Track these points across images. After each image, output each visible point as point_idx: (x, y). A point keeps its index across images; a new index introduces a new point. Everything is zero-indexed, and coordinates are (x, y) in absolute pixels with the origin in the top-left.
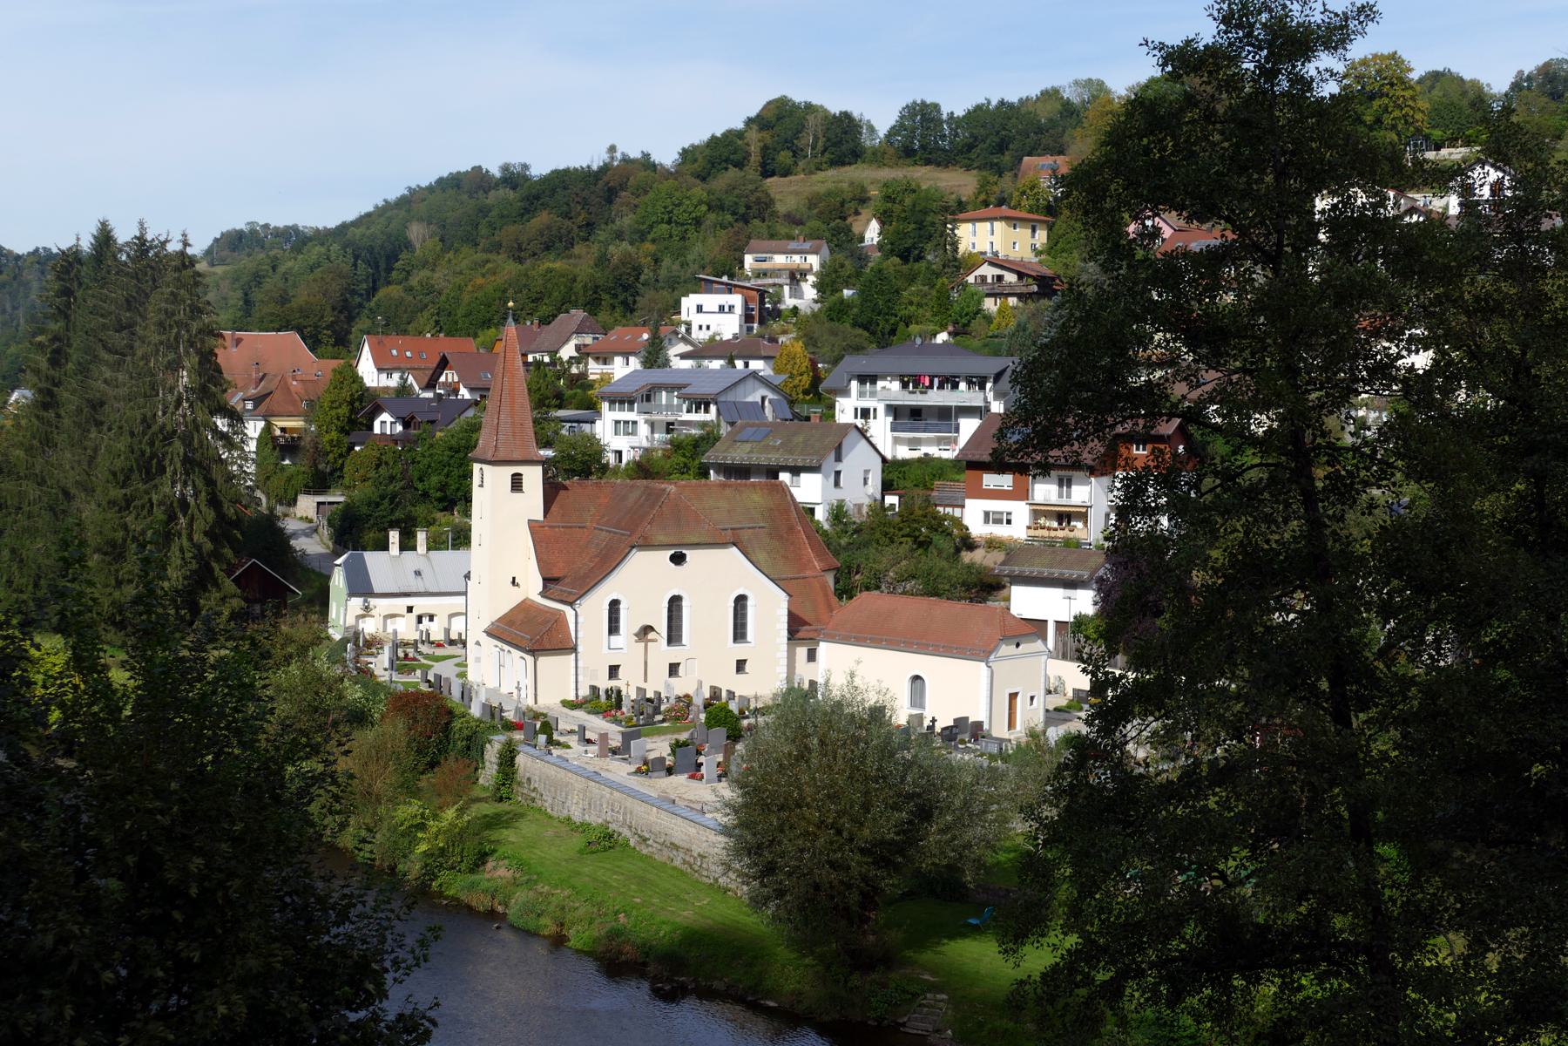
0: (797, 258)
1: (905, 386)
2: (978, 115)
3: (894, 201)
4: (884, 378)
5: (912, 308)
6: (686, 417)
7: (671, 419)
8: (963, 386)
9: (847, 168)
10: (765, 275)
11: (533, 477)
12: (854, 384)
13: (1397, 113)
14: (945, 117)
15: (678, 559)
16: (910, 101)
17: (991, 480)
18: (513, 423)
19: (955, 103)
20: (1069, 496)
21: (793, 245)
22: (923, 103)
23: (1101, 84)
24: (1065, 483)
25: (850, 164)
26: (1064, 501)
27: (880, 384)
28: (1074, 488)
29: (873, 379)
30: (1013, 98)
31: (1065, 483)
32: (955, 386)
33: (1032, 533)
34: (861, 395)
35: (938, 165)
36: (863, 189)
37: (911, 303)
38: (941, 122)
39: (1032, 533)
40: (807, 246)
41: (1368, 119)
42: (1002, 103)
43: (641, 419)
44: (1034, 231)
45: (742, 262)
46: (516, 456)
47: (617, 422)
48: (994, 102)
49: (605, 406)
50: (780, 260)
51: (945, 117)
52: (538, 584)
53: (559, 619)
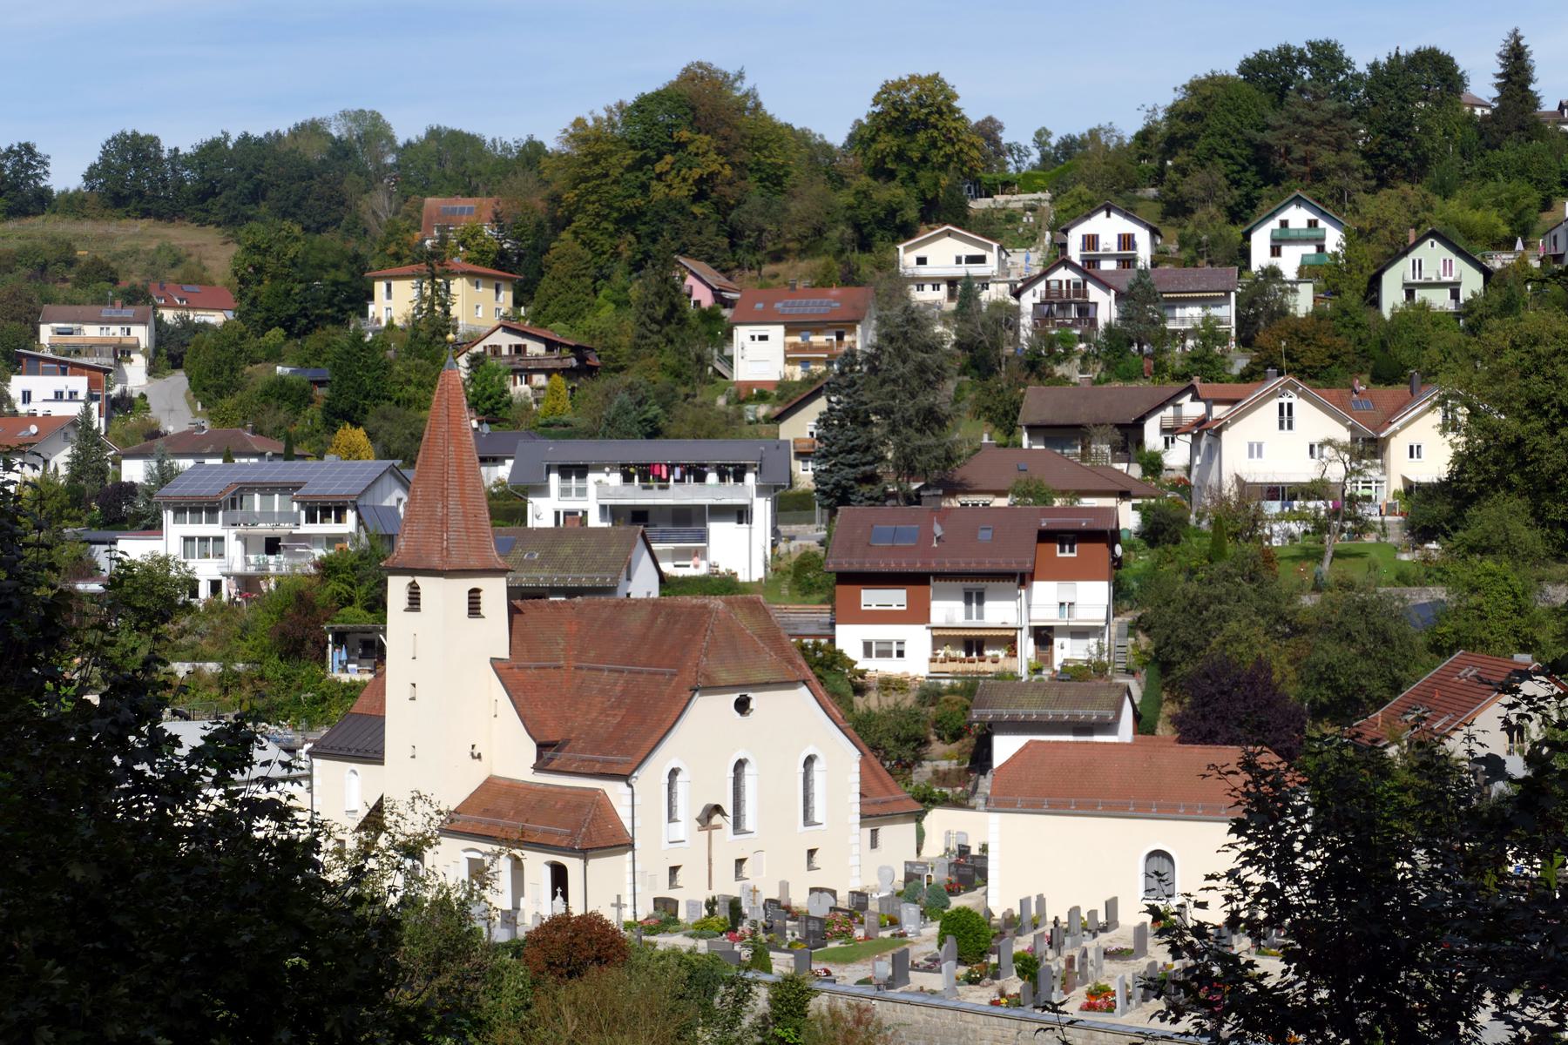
0: (116, 330)
1: (628, 478)
2: (212, 151)
3: (265, 252)
4: (599, 468)
5: (412, 389)
6: (306, 529)
7: (278, 532)
8: (712, 478)
9: (31, 220)
10: (78, 352)
11: (495, 592)
12: (554, 478)
13: (948, 149)
14: (165, 155)
15: (742, 706)
16: (117, 131)
17: (872, 598)
18: (465, 515)
19: (180, 135)
20: (980, 616)
21: (106, 312)
22: (135, 134)
23: (376, 117)
24: (975, 598)
25: (35, 214)
26: (974, 622)
27: (592, 477)
28: (988, 605)
29: (582, 471)
30: (258, 132)
31: (975, 598)
32: (700, 478)
33: (937, 667)
34: (565, 492)
35: (159, 217)
36: (70, 248)
37: (409, 382)
38: (158, 159)
39: (937, 667)
40: (129, 312)
41: (916, 155)
42: (245, 138)
43: (230, 534)
44: (498, 292)
45: (36, 333)
46: (474, 563)
47: (188, 539)
48: (745, 86)
49: (168, 516)
50: (92, 332)
51: (165, 155)
52: (530, 751)
53: (600, 803)
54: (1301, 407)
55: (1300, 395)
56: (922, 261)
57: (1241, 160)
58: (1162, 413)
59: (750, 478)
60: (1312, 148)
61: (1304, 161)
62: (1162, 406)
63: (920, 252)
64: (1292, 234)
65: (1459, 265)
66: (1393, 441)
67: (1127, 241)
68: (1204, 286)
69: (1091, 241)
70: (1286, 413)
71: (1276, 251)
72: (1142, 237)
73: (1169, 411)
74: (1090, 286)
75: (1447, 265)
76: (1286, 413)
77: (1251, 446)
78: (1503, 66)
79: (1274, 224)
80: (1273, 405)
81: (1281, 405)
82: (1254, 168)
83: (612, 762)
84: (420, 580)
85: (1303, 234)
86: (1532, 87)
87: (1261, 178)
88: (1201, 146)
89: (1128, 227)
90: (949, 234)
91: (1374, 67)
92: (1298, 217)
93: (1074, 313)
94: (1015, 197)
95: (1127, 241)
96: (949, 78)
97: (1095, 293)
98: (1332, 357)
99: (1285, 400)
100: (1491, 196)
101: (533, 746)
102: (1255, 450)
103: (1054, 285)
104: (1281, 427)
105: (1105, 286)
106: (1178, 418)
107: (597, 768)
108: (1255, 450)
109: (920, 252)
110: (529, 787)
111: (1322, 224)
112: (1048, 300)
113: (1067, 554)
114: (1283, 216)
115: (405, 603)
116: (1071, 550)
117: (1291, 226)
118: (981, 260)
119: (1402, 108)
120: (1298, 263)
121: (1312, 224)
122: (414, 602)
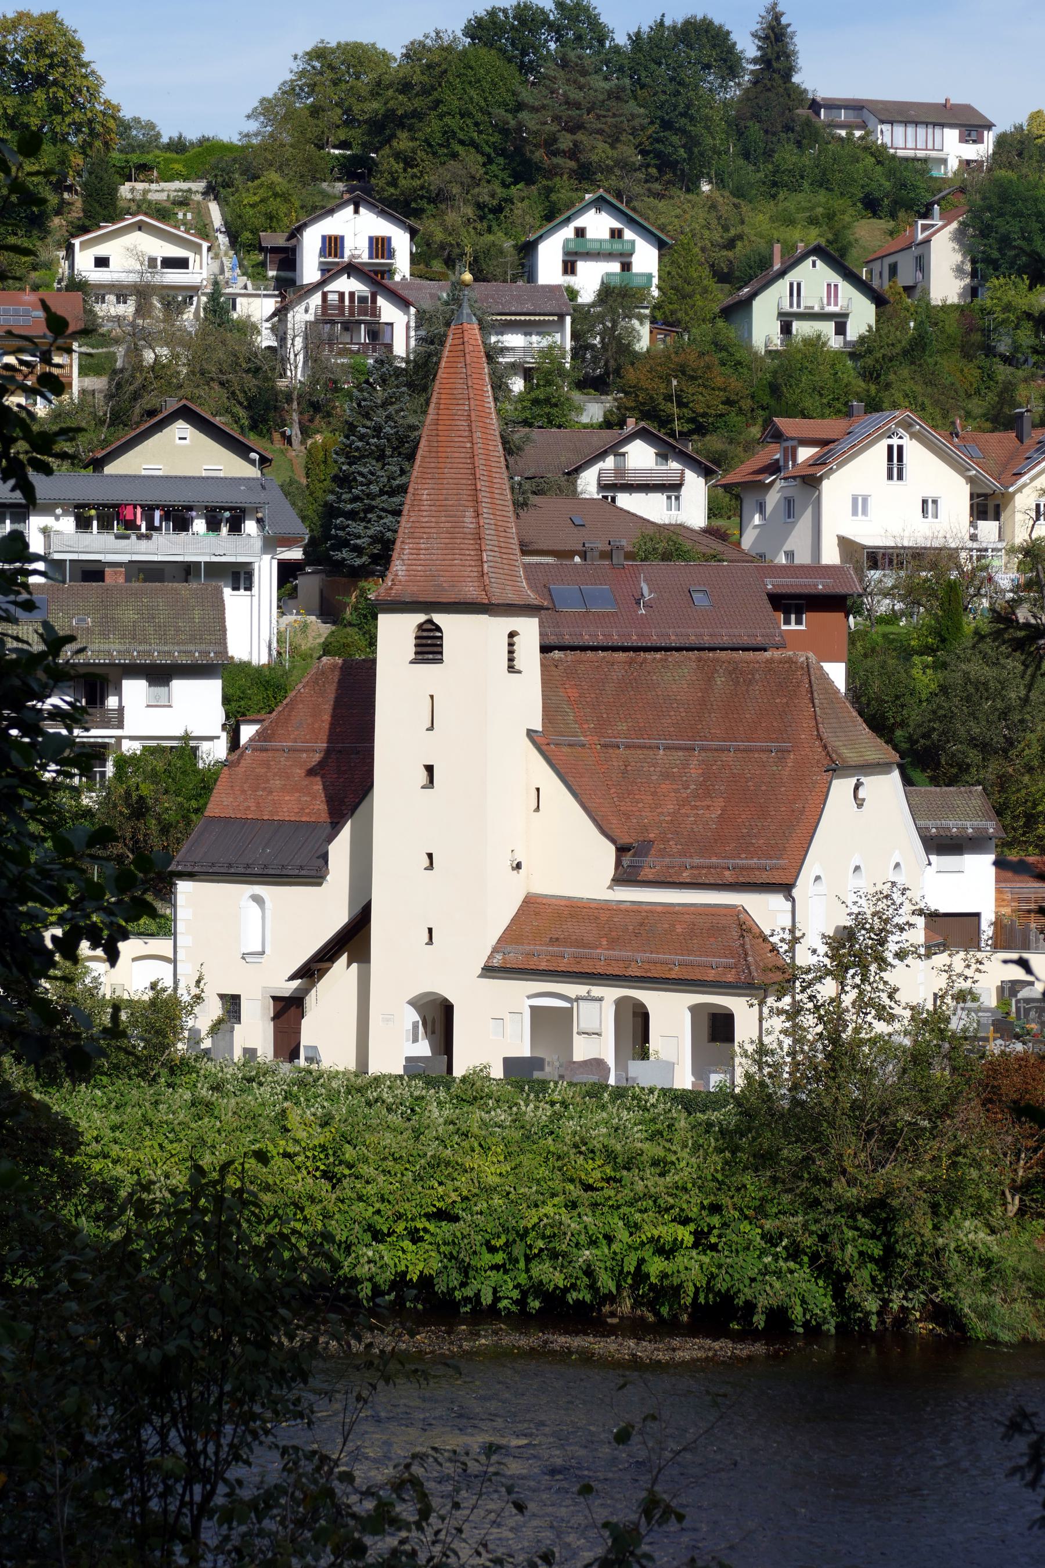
1: (83, 524)
8: (199, 525)
52: (604, 855)
53: (743, 926)
54: (915, 453)
55: (913, 436)
56: (102, 262)
57: (487, 149)
58: (600, 465)
59: (250, 526)
60: (580, 136)
61: (573, 154)
62: (602, 456)
63: (101, 250)
64: (590, 247)
65: (846, 290)
66: (1018, 497)
67: (381, 246)
68: (529, 307)
69: (333, 245)
70: (895, 458)
71: (569, 268)
72: (401, 242)
73: (609, 462)
74: (381, 301)
75: (832, 290)
76: (895, 458)
77: (855, 500)
78: (760, 48)
79: (568, 232)
80: (880, 450)
81: (890, 448)
82: (501, 160)
83: (743, 868)
84: (438, 618)
85: (607, 247)
86: (796, 79)
87: (536, 174)
88: (432, 127)
89: (383, 227)
90: (140, 227)
91: (636, 39)
92: (598, 224)
93: (363, 337)
94: (154, 186)
95: (381, 246)
96: (70, 19)
97: (388, 311)
98: (728, 402)
99: (895, 442)
100: (805, 209)
101: (612, 849)
102: (860, 505)
103: (333, 298)
104: (890, 477)
105: (402, 302)
106: (620, 471)
107: (729, 876)
108: (860, 505)
109: (101, 250)
110: (604, 907)
111: (629, 234)
112: (325, 316)
113: (793, 627)
114: (579, 222)
115: (409, 650)
116: (799, 622)
117: (589, 235)
118: (181, 263)
119: (677, 93)
120: (597, 286)
121: (616, 234)
122: (429, 647)
